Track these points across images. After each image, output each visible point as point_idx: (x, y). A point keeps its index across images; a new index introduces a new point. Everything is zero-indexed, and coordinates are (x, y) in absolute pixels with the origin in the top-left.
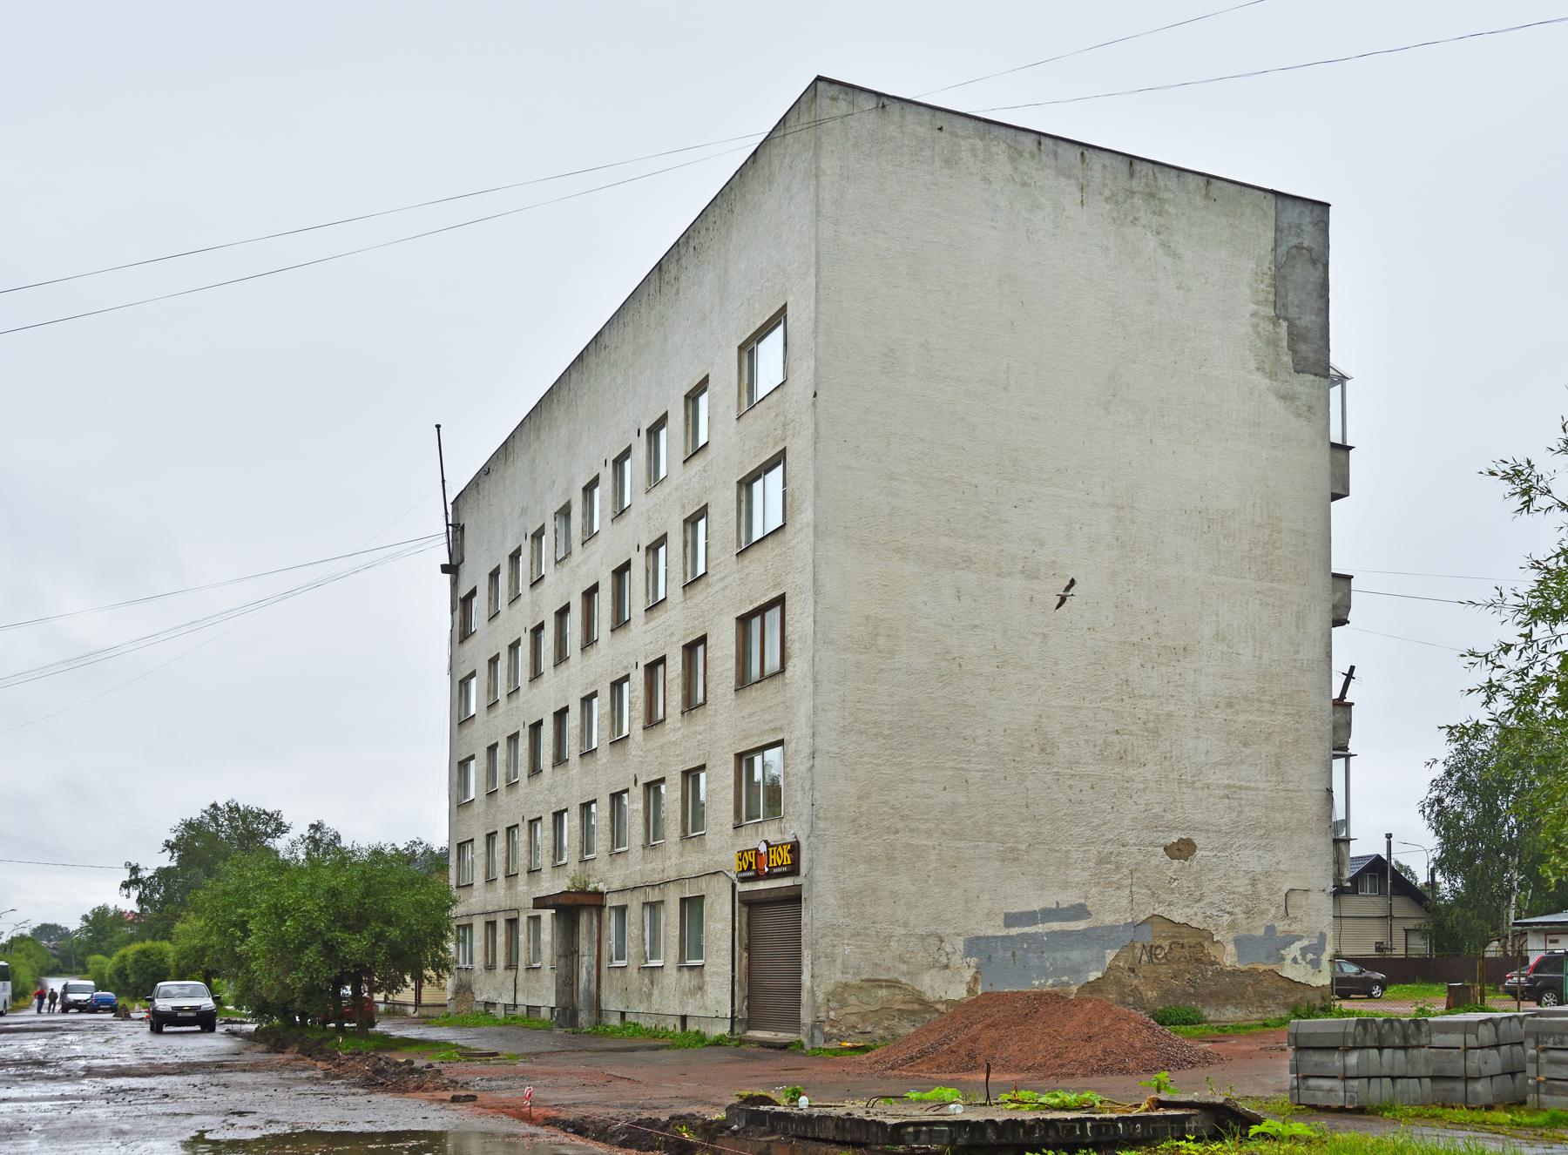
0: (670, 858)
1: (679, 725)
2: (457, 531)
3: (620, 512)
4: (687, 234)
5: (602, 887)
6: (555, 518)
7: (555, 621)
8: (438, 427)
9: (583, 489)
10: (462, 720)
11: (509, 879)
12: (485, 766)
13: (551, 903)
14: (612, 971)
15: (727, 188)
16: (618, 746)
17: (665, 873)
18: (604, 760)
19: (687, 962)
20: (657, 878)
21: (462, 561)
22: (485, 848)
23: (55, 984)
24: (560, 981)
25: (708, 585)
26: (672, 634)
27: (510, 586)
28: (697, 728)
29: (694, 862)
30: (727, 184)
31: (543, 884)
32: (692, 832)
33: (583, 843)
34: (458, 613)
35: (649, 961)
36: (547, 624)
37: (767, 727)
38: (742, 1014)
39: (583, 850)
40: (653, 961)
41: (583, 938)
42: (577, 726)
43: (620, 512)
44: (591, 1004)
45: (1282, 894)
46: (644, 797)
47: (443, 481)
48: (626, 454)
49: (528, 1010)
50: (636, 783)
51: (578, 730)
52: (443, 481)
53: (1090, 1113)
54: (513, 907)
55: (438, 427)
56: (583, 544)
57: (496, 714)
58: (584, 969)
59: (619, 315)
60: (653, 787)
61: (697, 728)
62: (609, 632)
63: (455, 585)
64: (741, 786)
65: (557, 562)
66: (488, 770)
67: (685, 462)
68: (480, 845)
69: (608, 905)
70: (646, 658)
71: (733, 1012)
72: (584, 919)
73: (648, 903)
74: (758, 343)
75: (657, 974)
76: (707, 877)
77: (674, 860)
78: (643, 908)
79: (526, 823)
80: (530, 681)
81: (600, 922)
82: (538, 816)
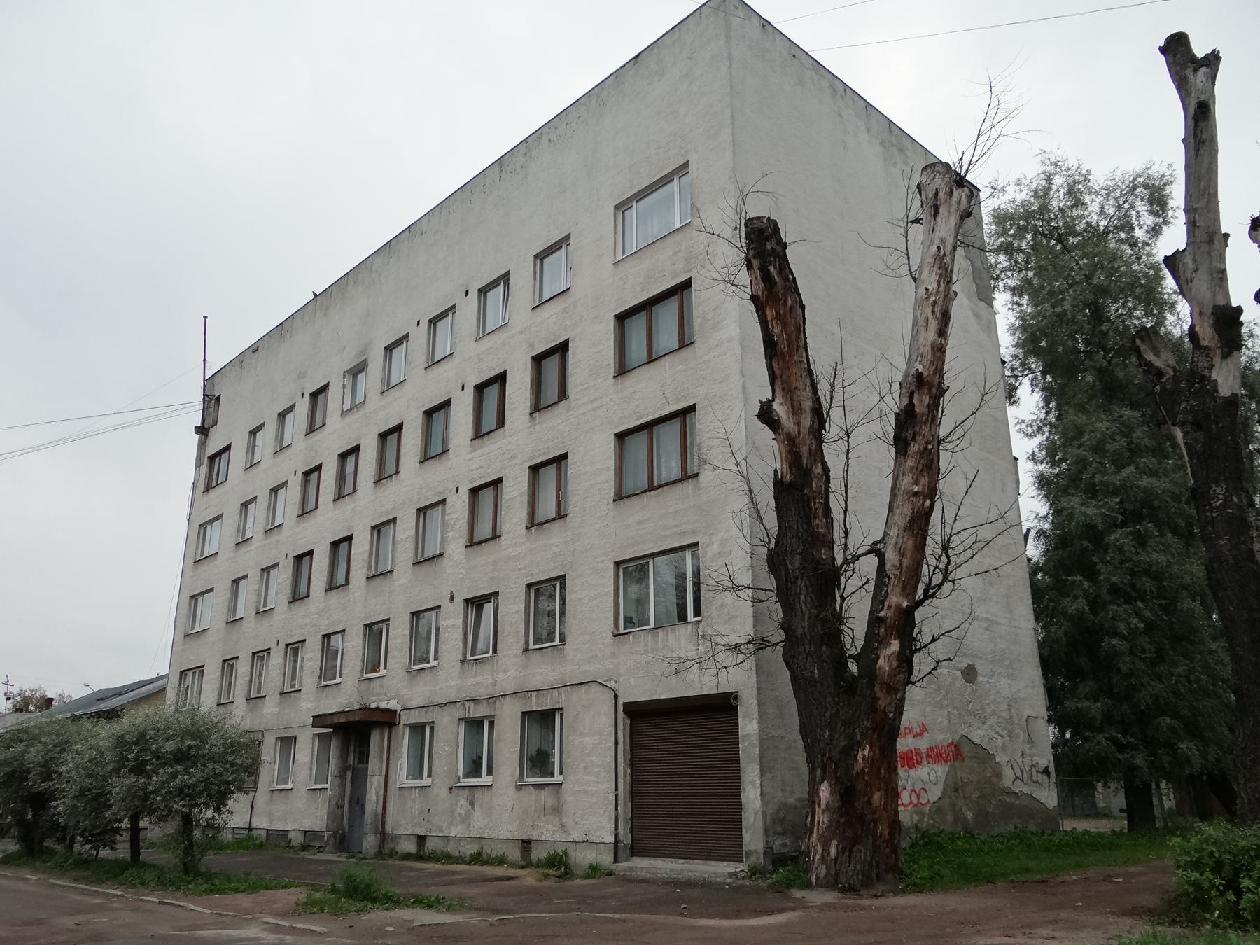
0: (505, 671)
1: (524, 540)
2: (211, 400)
3: (281, 449)
4: (539, 132)
5: (392, 705)
6: (344, 376)
7: (532, 367)
8: (205, 318)
9: (479, 290)
10: (199, 559)
11: (251, 701)
12: (228, 596)
13: (329, 722)
14: (406, 793)
15: (668, 40)
16: (426, 567)
17: (497, 688)
18: (403, 581)
19: (526, 780)
20: (483, 692)
21: (215, 423)
22: (220, 673)
24: (334, 802)
25: (569, 408)
27: (276, 439)
28: (552, 541)
29: (481, 681)
30: (597, 86)
32: (471, 656)
33: (363, 662)
34: (205, 468)
35: (461, 780)
36: (696, 283)
38: (625, 836)
39: (363, 670)
40: (466, 780)
41: (374, 757)
42: (522, 494)
43: (281, 449)
45: (1024, 719)
46: (464, 612)
47: (205, 360)
48: (290, 409)
49: (267, 834)
50: (452, 599)
51: (366, 556)
52: (205, 360)
53: (454, 873)
54: (256, 727)
55: (205, 318)
56: (382, 393)
57: (248, 549)
58: (373, 791)
59: (441, 208)
60: (294, 648)
61: (552, 541)
62: (418, 465)
63: (202, 445)
64: (618, 597)
65: (343, 412)
66: (231, 599)
67: (426, 369)
68: (213, 673)
69: (402, 722)
70: (472, 482)
71: (616, 836)
73: (462, 719)
75: (479, 794)
76: (568, 687)
77: (511, 673)
78: (459, 724)
79: (282, 646)
80: (335, 501)
81: (389, 740)
82: (302, 638)
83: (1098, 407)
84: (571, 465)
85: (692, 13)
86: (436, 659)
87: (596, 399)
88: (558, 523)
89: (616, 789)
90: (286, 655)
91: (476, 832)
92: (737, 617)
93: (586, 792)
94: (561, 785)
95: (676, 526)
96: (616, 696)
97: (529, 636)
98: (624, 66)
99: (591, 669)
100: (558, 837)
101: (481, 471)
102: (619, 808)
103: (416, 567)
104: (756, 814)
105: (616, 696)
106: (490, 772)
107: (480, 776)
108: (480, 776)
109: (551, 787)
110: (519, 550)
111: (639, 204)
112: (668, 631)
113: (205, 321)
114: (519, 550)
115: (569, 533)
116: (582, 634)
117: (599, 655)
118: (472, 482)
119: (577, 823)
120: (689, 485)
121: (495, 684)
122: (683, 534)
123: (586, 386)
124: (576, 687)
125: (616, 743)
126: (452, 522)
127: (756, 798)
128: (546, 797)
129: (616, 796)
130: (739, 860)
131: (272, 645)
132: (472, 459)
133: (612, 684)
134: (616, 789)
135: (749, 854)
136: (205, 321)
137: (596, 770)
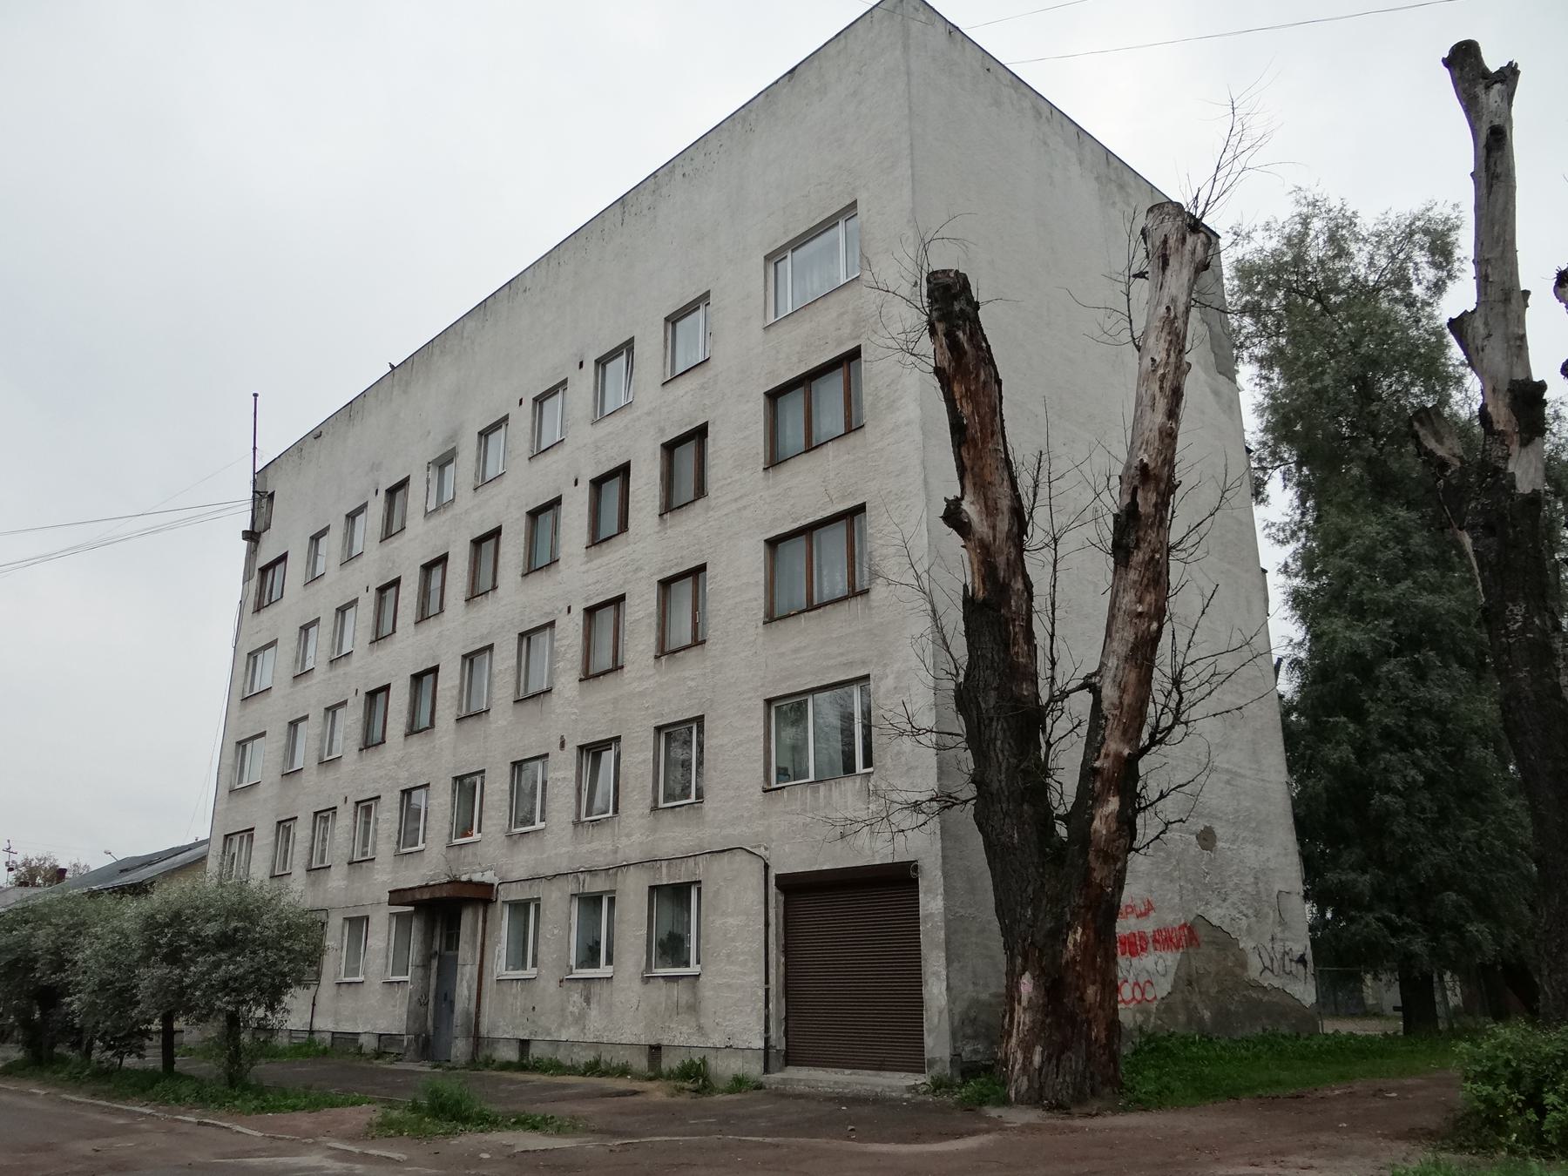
0: (628, 836)
1: (652, 671)
2: (263, 498)
3: (349, 559)
4: (671, 165)
5: (488, 877)
6: (428, 468)
7: (662, 457)
8: (256, 395)
9: (596, 361)
11: (312, 873)
12: (284, 742)
13: (410, 899)
14: (505, 986)
15: (832, 50)
16: (530, 706)
18: (502, 723)
19: (654, 970)
20: (600, 862)
21: (268, 527)
22: (274, 838)
23: (1027, 985)
24: (415, 999)
26: (637, 570)
27: (344, 546)
28: (687, 674)
29: (598, 848)
30: (743, 107)
31: (376, 877)
32: (587, 816)
33: (452, 824)
34: (255, 582)
35: (574, 971)
36: (866, 352)
37: (832, 662)
38: (778, 1040)
39: (451, 833)
40: (580, 971)
41: (465, 942)
43: (349, 559)
44: (469, 1031)
46: (577, 762)
47: (255, 448)
48: (361, 509)
49: (333, 1038)
50: (562, 745)
51: (455, 692)
52: (255, 448)
54: (319, 905)
55: (256, 395)
56: (475, 489)
57: (309, 683)
58: (465, 984)
60: (366, 807)
61: (687, 674)
62: (520, 578)
63: (252, 554)
64: (770, 743)
65: (426, 513)
66: (287, 746)
67: (530, 459)
68: (264, 837)
69: (501, 899)
70: (587, 600)
71: (767, 1040)
72: (467, 918)
73: (575, 895)
74: (793, 251)
75: (596, 988)
76: (707, 855)
77: (636, 838)
78: (571, 901)
80: (416, 623)
81: (485, 921)
82: (376, 795)
83: (1367, 507)
84: (710, 578)
85: (861, 17)
86: (542, 820)
87: (741, 497)
88: (695, 651)
89: (767, 982)
90: (356, 815)
91: (592, 1036)
92: (917, 767)
93: (729, 986)
94: (698, 976)
95: (842, 654)
96: (767, 867)
97: (658, 791)
98: (777, 82)
99: (736, 833)
100: (694, 1041)
101: (599, 586)
102: (770, 1006)
103: (518, 705)
104: (940, 1013)
105: (767, 867)
106: (609, 961)
107: (598, 966)
108: (598, 966)
109: (685, 979)
110: (646, 685)
111: (795, 253)
112: (831, 785)
113: (256, 400)
114: (646, 685)
115: (708, 663)
116: (724, 789)
117: (746, 815)
118: (587, 600)
119: (717, 1024)
120: (857, 604)
121: (615, 852)
122: (850, 664)
123: (729, 480)
124: (717, 855)
125: (767, 925)
126: (563, 649)
127: (941, 993)
128: (679, 992)
129: (767, 991)
130: (920, 1070)
131: (339, 803)
132: (587, 571)
133: (761, 851)
134: (767, 982)
135: (932, 1063)
136: (256, 400)
137: (742, 958)
